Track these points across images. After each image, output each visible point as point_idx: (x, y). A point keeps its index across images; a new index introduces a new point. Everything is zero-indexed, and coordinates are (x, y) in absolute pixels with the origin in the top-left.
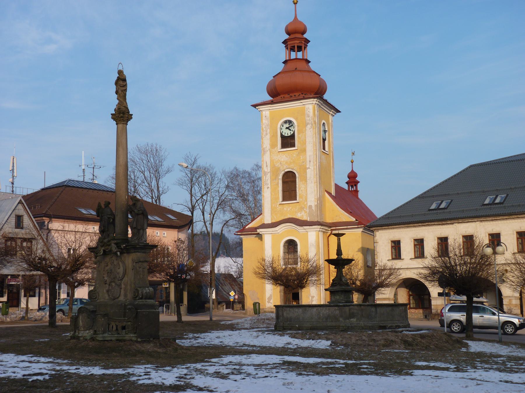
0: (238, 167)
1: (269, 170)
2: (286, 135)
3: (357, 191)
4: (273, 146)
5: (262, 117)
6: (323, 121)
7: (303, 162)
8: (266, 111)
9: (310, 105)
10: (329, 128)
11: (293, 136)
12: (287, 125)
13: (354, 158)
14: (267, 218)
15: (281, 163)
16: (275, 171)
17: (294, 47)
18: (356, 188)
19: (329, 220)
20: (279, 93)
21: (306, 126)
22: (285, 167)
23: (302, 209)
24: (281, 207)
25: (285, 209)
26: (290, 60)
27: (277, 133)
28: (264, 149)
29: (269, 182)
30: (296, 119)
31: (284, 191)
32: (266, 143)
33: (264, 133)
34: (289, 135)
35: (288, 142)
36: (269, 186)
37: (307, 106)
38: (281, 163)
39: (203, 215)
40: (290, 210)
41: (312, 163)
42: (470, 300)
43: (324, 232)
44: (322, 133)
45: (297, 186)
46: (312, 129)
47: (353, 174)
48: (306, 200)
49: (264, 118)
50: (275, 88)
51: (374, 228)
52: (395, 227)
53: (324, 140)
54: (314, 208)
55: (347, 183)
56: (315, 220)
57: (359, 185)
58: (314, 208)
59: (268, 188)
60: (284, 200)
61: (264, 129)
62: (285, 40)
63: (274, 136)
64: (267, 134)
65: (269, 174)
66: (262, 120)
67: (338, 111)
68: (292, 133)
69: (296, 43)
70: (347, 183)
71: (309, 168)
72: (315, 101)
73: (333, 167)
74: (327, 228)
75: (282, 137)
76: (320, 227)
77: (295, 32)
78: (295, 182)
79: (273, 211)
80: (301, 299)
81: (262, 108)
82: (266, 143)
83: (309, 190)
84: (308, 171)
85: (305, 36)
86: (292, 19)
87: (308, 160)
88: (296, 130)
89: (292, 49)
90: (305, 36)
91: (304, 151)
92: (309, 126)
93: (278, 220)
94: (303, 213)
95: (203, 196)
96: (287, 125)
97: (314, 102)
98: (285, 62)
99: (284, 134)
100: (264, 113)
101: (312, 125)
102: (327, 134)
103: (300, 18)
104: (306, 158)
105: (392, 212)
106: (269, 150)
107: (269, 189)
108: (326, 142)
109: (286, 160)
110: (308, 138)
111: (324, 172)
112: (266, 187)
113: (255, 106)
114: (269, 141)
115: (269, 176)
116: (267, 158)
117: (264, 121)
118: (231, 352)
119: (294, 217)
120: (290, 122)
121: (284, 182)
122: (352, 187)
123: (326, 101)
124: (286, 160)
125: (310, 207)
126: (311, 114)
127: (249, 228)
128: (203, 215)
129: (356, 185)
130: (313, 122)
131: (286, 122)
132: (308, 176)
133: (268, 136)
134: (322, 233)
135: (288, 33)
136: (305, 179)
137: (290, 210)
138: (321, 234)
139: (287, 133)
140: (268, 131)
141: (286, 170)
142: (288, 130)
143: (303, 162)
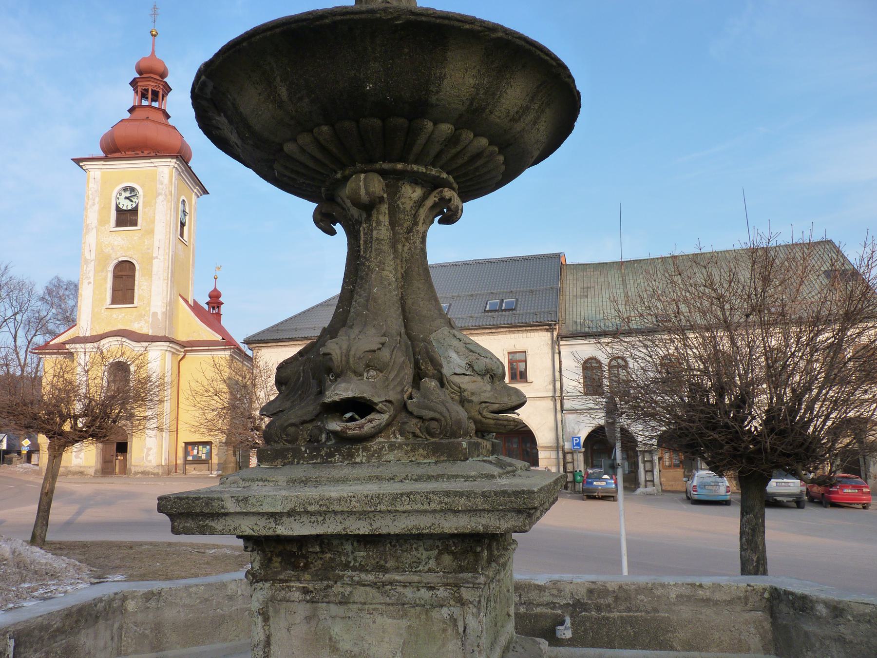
0: (60, 276)
1: (93, 257)
2: (125, 208)
3: (219, 315)
4: (103, 222)
5: (88, 179)
6: (183, 198)
7: (148, 249)
8: (96, 170)
9: (165, 169)
10: (190, 210)
11: (135, 211)
12: (128, 194)
13: (219, 273)
14: (85, 326)
15: (113, 249)
16: (102, 258)
17: (147, 90)
18: (219, 310)
19: (182, 337)
20: (115, 148)
21: (157, 197)
22: (119, 254)
23: (141, 317)
24: (108, 312)
25: (114, 316)
26: (140, 106)
27: (110, 203)
28: (87, 226)
29: (91, 274)
30: (142, 186)
31: (114, 290)
32: (92, 216)
33: (90, 202)
34: (130, 208)
35: (126, 217)
36: (92, 280)
37: (160, 169)
38: (113, 249)
39: (15, 341)
40: (123, 317)
41: (161, 251)
42: (529, 467)
43: (173, 353)
44: (180, 213)
45: (136, 282)
46: (165, 202)
47: (215, 294)
48: (149, 304)
49: (91, 180)
50: (113, 141)
51: (254, 345)
52: (287, 343)
53: (183, 225)
54: (160, 317)
55: (207, 303)
56: (161, 334)
57: (222, 307)
58: (160, 317)
59: (89, 283)
60: (113, 303)
61: (91, 197)
62: (135, 79)
63: (104, 208)
64: (94, 204)
65: (93, 263)
66: (88, 182)
67: (206, 192)
68: (134, 205)
69: (151, 86)
70: (207, 303)
71: (157, 258)
72: (173, 162)
73: (193, 265)
74: (178, 348)
75: (119, 211)
76: (168, 344)
77: (151, 71)
78: (133, 277)
79: (95, 316)
80: (131, 452)
81: (87, 165)
82: (92, 216)
83: (153, 289)
84: (155, 261)
85: (165, 80)
86: (148, 54)
87: (156, 245)
88: (141, 201)
89: (144, 96)
90: (165, 80)
91: (151, 232)
92: (161, 198)
93: (101, 332)
94: (143, 323)
95: (15, 314)
96: (128, 194)
97: (173, 164)
98: (131, 110)
99: (121, 206)
100: (92, 173)
101: (166, 196)
102: (187, 217)
103: (158, 56)
104: (152, 246)
105: (282, 323)
106: (96, 227)
107: (91, 285)
108: (186, 229)
109: (123, 244)
110: (159, 216)
111: (179, 272)
112: (86, 282)
113: (77, 161)
114: (97, 216)
115: (92, 266)
116: (91, 239)
117: (91, 185)
118: (354, 283)
119: (127, 328)
120: (132, 189)
121: (115, 277)
122: (214, 308)
123: (190, 168)
124: (123, 244)
125: (155, 314)
126: (166, 180)
127: (55, 344)
128: (15, 341)
129: (218, 307)
130: (167, 193)
131: (125, 189)
132: (155, 269)
133: (96, 208)
134: (170, 354)
135: (140, 72)
136: (149, 274)
137: (123, 317)
138: (168, 356)
139: (126, 205)
140: (97, 199)
141: (120, 259)
142: (127, 201)
143: (148, 249)
